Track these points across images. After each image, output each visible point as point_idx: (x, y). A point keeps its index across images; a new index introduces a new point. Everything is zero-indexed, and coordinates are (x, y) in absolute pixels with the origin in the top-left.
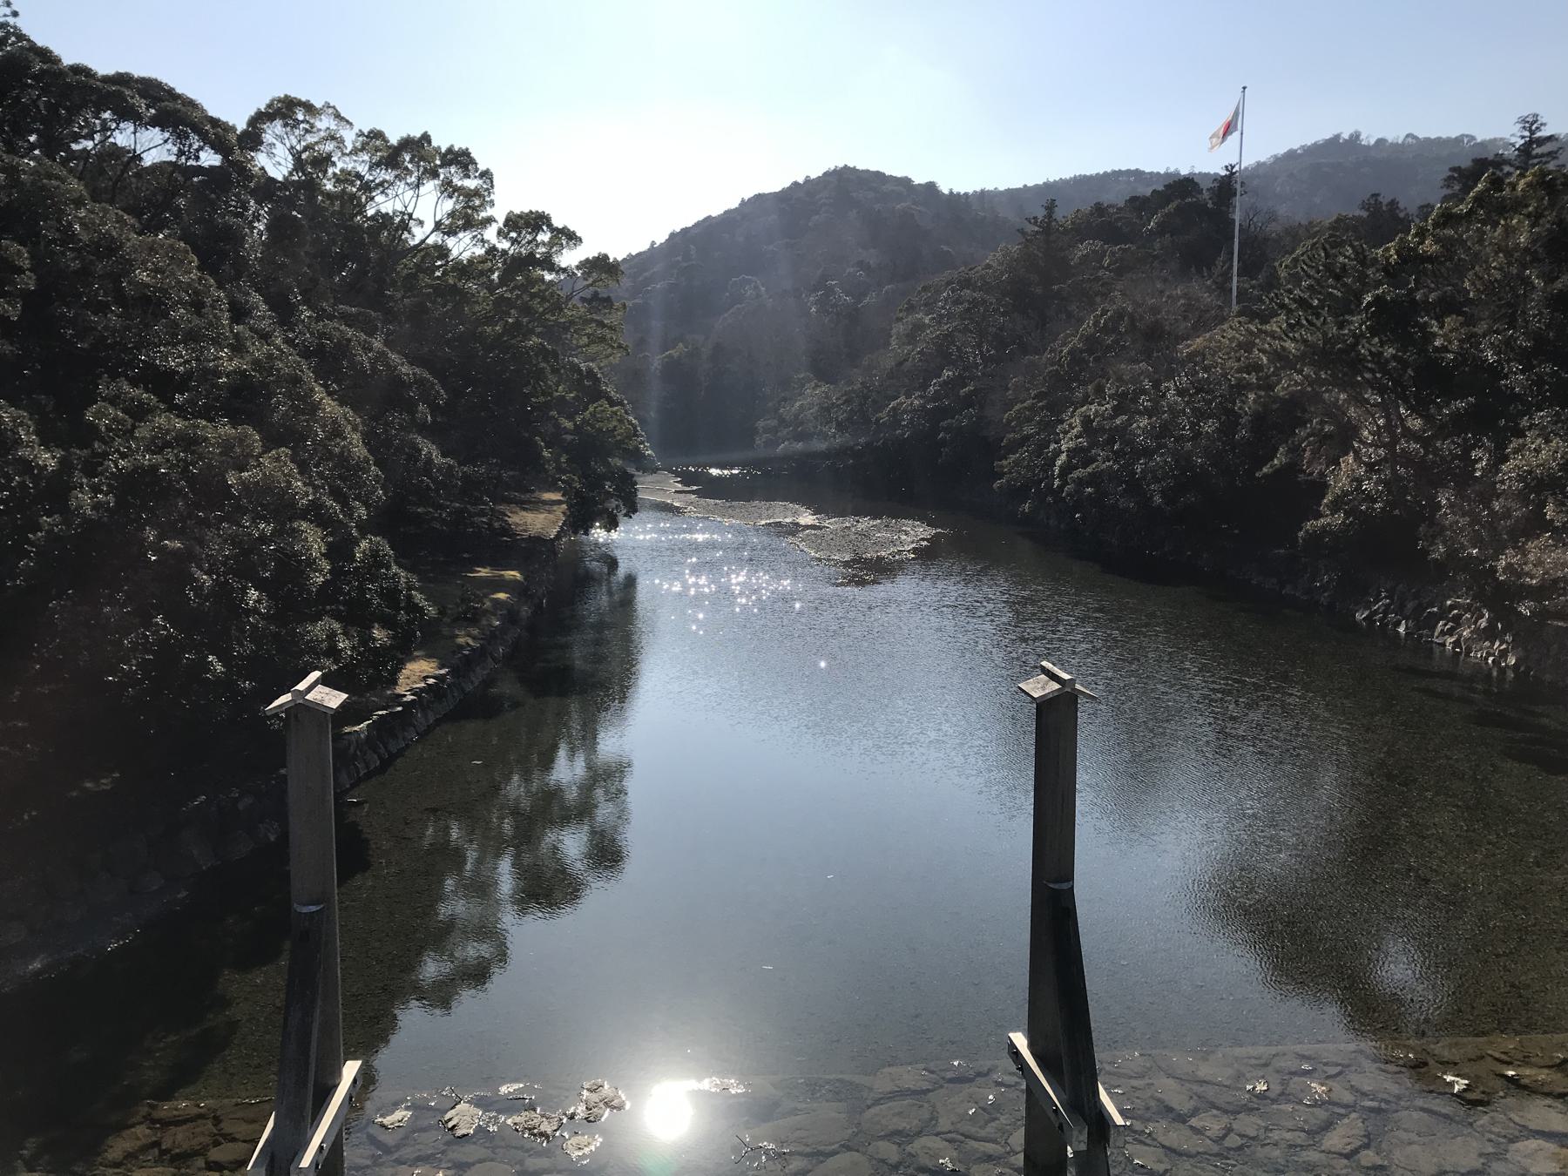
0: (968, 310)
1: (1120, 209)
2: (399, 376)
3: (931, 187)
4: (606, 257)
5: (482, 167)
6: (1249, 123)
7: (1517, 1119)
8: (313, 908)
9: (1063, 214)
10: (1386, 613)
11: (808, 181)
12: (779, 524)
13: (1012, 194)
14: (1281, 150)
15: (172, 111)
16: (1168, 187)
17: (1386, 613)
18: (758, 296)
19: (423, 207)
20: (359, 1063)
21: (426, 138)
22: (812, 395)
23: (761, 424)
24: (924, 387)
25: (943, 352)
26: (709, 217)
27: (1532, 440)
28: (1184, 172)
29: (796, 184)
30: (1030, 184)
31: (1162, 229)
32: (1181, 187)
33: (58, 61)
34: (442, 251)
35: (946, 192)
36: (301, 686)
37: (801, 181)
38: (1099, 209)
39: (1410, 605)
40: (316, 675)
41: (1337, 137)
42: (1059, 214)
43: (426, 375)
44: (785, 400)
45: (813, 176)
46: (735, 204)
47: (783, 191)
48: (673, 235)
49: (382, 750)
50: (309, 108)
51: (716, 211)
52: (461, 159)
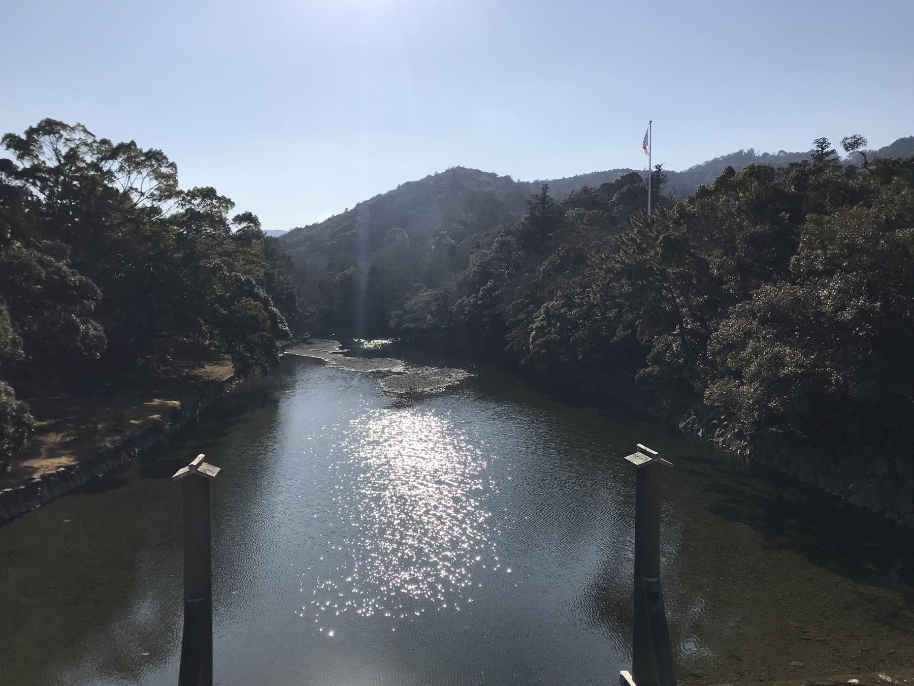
1: (598, 191)
2: (66, 282)
3: (508, 178)
4: (250, 214)
5: (170, 161)
8: (197, 600)
10: (693, 424)
11: (437, 175)
12: (379, 372)
14: (711, 159)
17: (693, 424)
18: (404, 239)
19: (140, 186)
21: (133, 143)
22: (425, 295)
23: (393, 313)
24: (477, 292)
25: (484, 273)
26: (379, 196)
27: (733, 320)
29: (429, 176)
30: (566, 177)
31: (619, 200)
34: (156, 211)
35: (516, 181)
36: (194, 463)
38: (586, 190)
39: (704, 420)
40: (201, 456)
41: (741, 152)
43: (90, 281)
44: (408, 299)
45: (440, 172)
46: (394, 187)
47: (422, 180)
50: (64, 126)
51: (384, 191)
52: (155, 156)
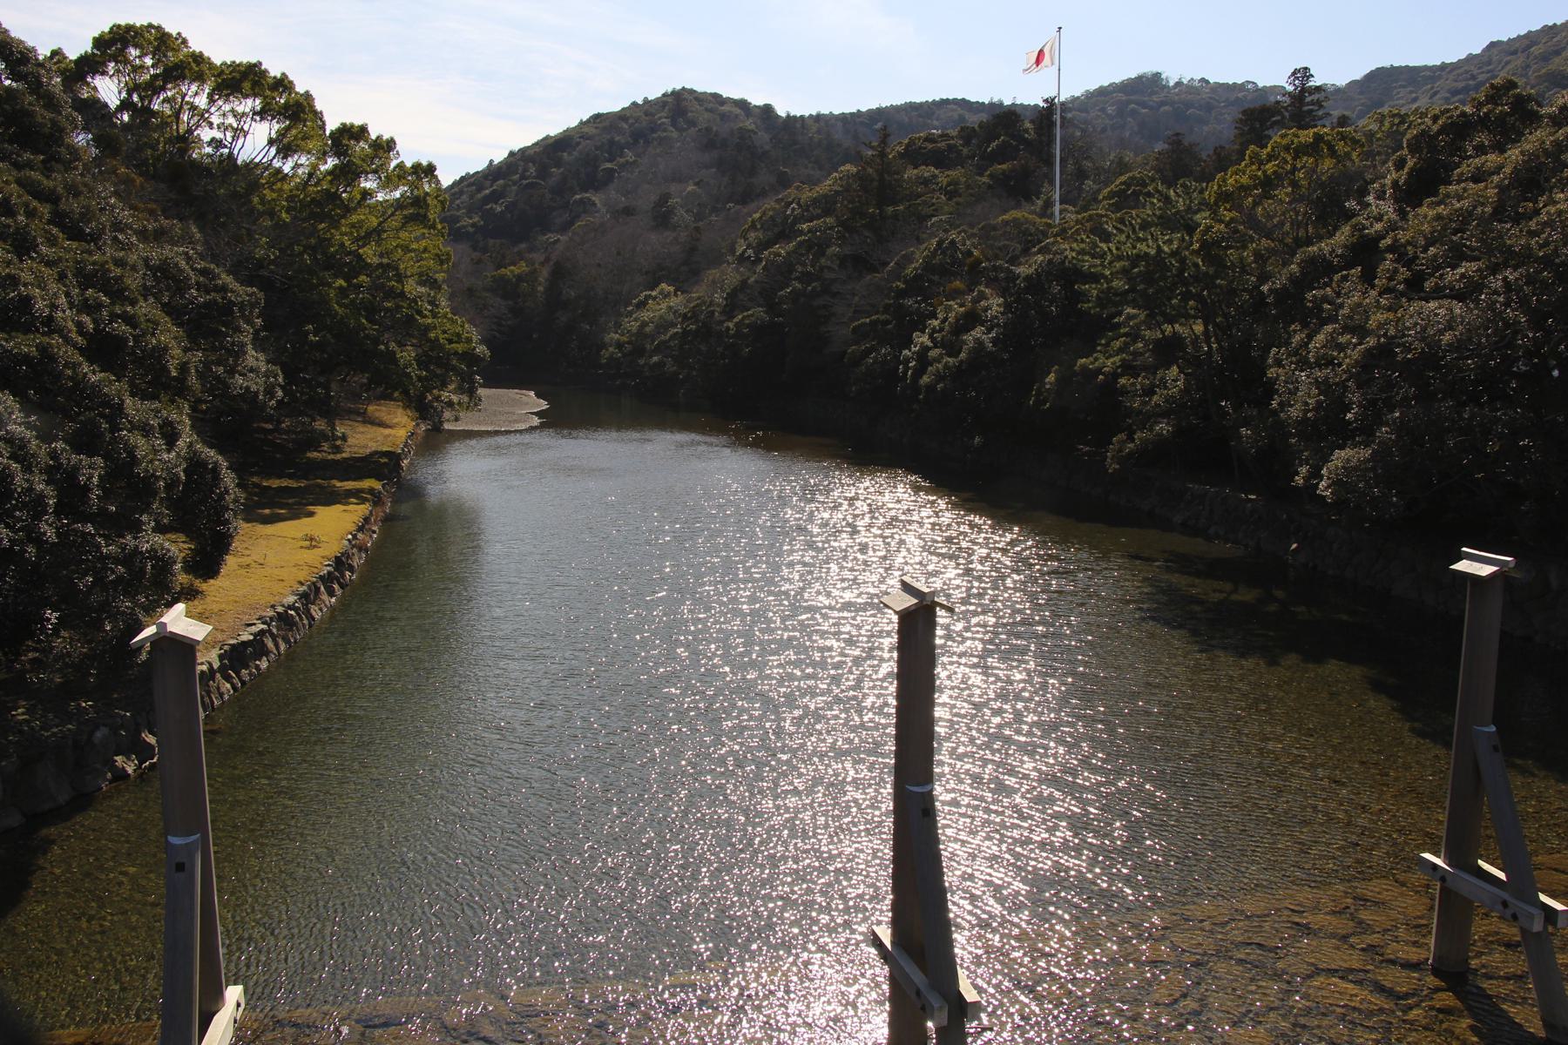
13: (844, 118)
14: (1093, 86)
15: (293, 111)
28: (1007, 102)
29: (634, 104)
32: (1004, 119)
35: (783, 115)
49: (236, 680)
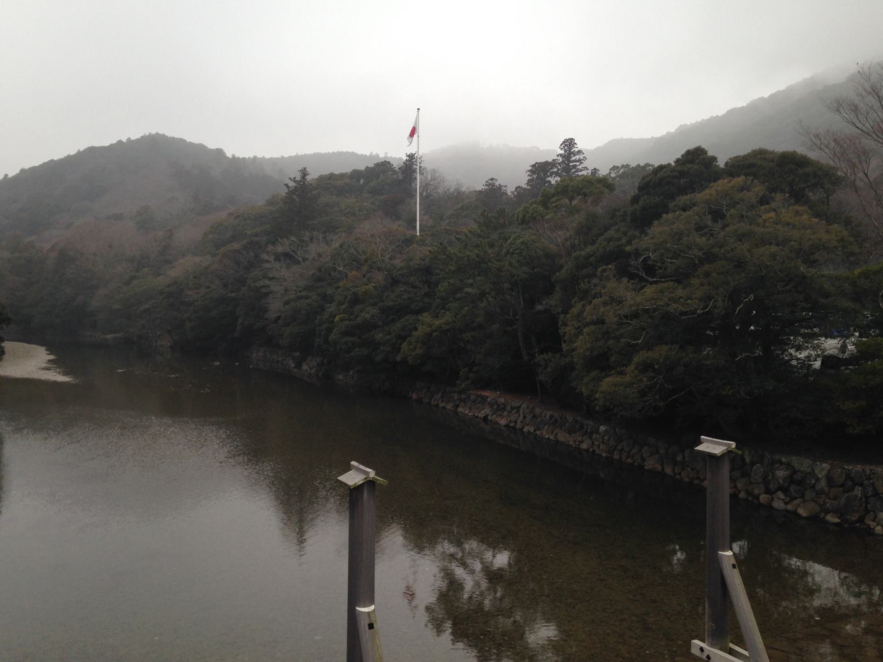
0: (672, 197)
6: (421, 130)
7: (823, 154)
9: (313, 175)
16: (377, 165)
20: (339, 478)
26: (52, 161)
32: (383, 167)
33: (669, 165)
37: (124, 140)
42: (308, 178)
48: (23, 171)
